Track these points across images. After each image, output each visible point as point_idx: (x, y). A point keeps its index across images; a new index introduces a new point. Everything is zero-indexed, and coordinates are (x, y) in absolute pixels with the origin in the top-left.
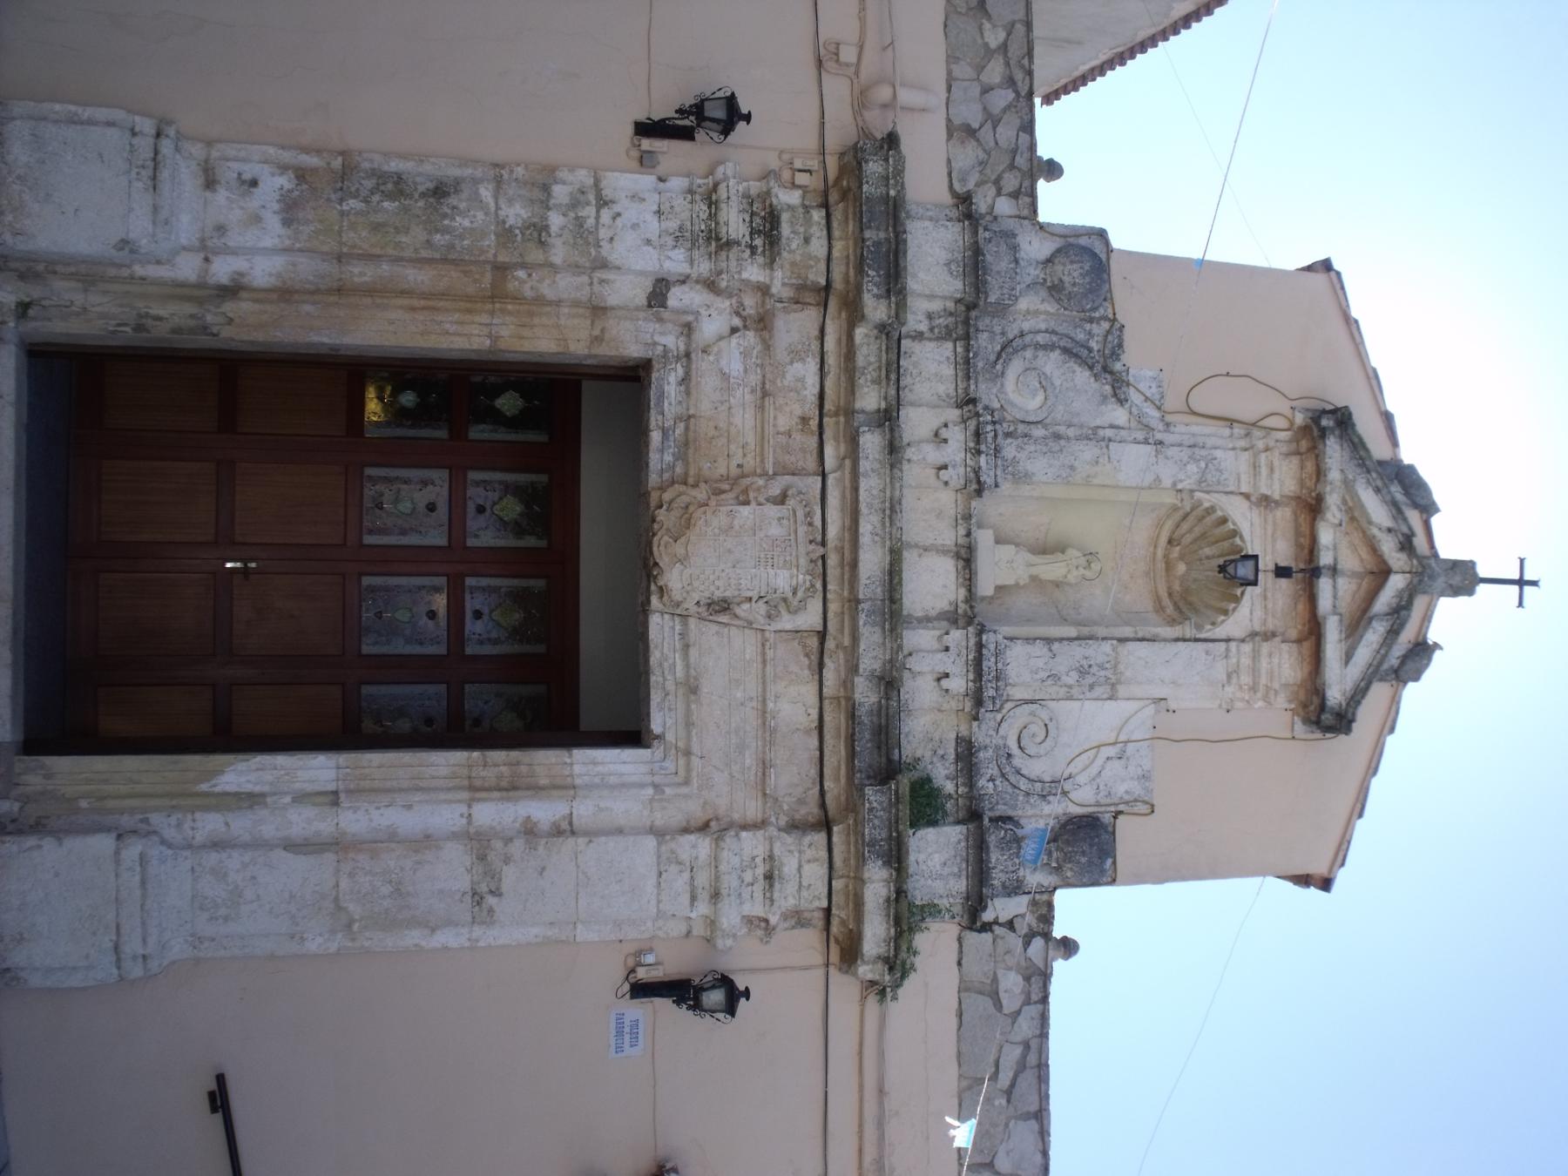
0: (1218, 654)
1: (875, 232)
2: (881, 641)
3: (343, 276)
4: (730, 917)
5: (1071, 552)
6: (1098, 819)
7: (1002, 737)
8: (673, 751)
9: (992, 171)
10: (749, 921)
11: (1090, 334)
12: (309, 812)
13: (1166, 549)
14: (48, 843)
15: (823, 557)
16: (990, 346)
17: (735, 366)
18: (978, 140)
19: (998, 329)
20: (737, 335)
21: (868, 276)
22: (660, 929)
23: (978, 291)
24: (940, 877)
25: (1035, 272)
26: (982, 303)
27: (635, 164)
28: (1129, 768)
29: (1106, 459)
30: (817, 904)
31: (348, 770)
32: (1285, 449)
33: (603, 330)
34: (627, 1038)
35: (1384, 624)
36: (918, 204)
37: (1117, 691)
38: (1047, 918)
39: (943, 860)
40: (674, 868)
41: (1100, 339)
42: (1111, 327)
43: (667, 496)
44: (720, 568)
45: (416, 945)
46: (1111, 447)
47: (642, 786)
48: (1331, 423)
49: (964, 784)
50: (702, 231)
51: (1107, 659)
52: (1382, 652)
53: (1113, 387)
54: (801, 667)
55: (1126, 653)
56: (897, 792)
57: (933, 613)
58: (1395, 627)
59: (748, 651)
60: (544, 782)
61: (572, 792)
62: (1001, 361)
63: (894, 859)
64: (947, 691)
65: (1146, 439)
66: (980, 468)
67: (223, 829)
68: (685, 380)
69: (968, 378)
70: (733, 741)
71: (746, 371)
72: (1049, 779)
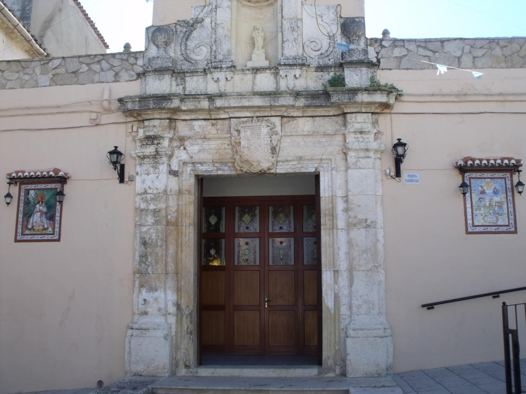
2: (284, 98)
4: (374, 145)
5: (254, 35)
6: (342, 24)
7: (315, 57)
8: (321, 164)
10: (376, 139)
12: (340, 279)
14: (349, 357)
15: (257, 117)
17: (196, 148)
18: (119, 72)
19: (181, 62)
20: (186, 147)
21: (165, 106)
22: (378, 168)
23: (168, 70)
24: (361, 76)
25: (161, 51)
26: (172, 68)
27: (133, 182)
31: (327, 267)
33: (186, 191)
34: (413, 178)
36: (141, 91)
37: (300, 18)
38: (376, 40)
40: (358, 164)
41: (182, 28)
42: (178, 24)
43: (238, 168)
45: (383, 246)
46: (218, 23)
47: (332, 174)
49: (331, 69)
50: (153, 160)
51: (289, 22)
53: (198, 23)
54: (293, 123)
55: (286, 16)
57: (275, 81)
59: (288, 141)
61: (334, 197)
62: (191, 61)
64: (300, 75)
65: (215, 11)
66: (226, 67)
68: (201, 164)
69: (197, 72)
70: (317, 145)
71: (198, 144)
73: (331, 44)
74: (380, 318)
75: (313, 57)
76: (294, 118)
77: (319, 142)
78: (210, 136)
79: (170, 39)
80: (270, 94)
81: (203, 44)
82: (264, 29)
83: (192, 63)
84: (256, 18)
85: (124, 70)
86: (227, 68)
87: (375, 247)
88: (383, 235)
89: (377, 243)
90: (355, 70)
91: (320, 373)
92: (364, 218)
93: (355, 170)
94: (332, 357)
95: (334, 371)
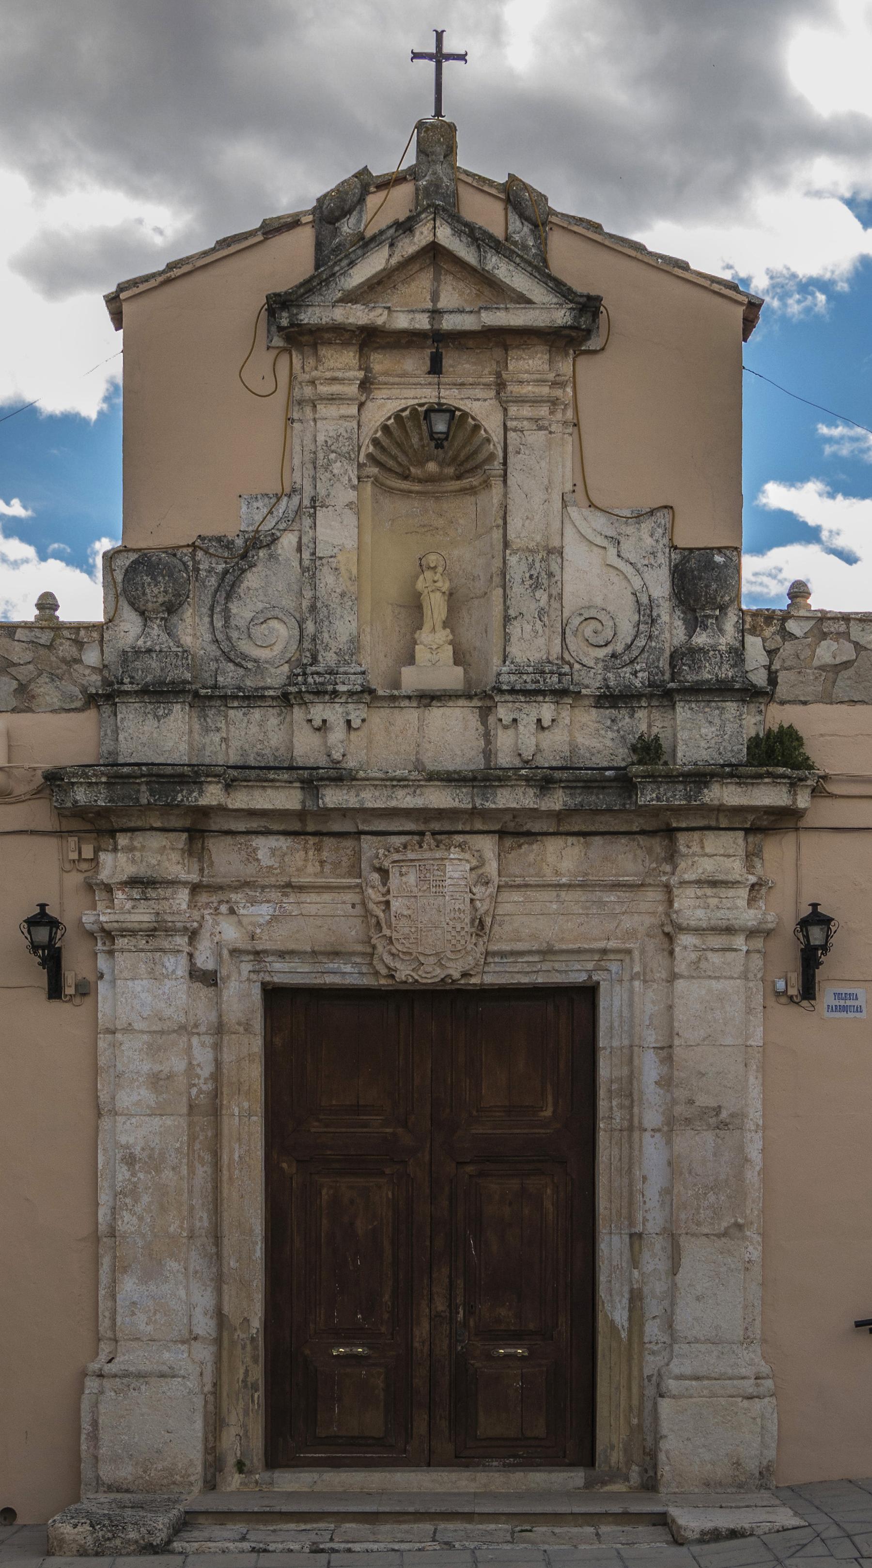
0: (519, 440)
1: (141, 795)
2: (510, 789)
3: (204, 1234)
4: (749, 917)
5: (420, 585)
6: (676, 566)
7: (596, 663)
8: (602, 963)
9: (59, 668)
10: (751, 901)
11: (210, 571)
12: (646, 1255)
13: (414, 481)
14: (664, 1445)
15: (434, 834)
16: (231, 674)
17: (264, 911)
18: (30, 682)
19: (213, 666)
20: (236, 909)
21: (182, 800)
22: (755, 975)
23: (183, 691)
24: (722, 726)
25: (155, 630)
26: (194, 687)
27: (88, 1000)
28: (628, 532)
29: (332, 559)
30: (741, 841)
31: (613, 1226)
32: (312, 361)
33: (239, 1024)
34: (849, 1003)
35: (489, 255)
36: (100, 744)
37: (555, 548)
38: (769, 617)
39: (707, 724)
40: (703, 965)
41: (214, 561)
42: (201, 549)
43: (384, 971)
44: (446, 926)
45: (759, 1174)
46: (321, 555)
47: (631, 992)
48: (285, 314)
49: (639, 701)
50: (147, 942)
51: (524, 561)
52: (518, 260)
53: (260, 548)
54: (531, 852)
55: (518, 540)
56: (643, 777)
57: (481, 729)
58: (492, 245)
59: (516, 899)
60: (625, 1071)
61: (636, 1049)
62: (243, 663)
63: (703, 779)
64: (553, 721)
65: (310, 516)
66: (349, 691)
67: (658, 1320)
68: (282, 954)
69: (263, 697)
70: (595, 911)
71: (268, 902)
72: (636, 617)
73: (642, 627)
74: (745, 1352)
75: (591, 664)
76: (533, 838)
77: (601, 903)
78: (304, 880)
79: (180, 596)
80: (474, 779)
81: (277, 613)
82: (448, 562)
83: (246, 669)
84: (424, 526)
85: (44, 678)
86: (351, 693)
87: (740, 1176)
88: (761, 1147)
89: (743, 1167)
90: (707, 710)
91: (589, 1484)
92: (713, 1104)
93: (694, 981)
94: (621, 1445)
95: (627, 1479)
